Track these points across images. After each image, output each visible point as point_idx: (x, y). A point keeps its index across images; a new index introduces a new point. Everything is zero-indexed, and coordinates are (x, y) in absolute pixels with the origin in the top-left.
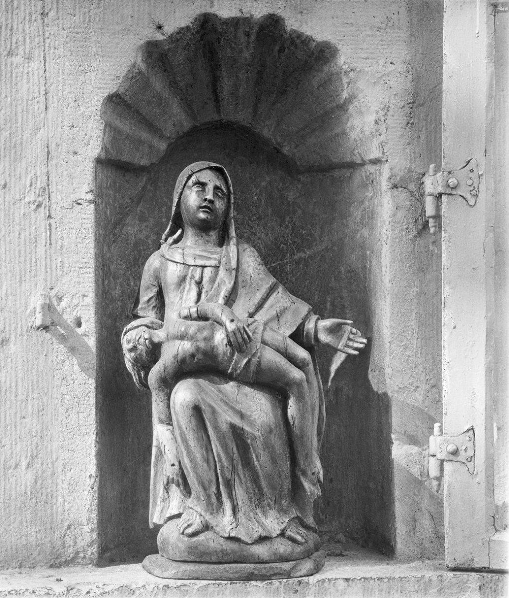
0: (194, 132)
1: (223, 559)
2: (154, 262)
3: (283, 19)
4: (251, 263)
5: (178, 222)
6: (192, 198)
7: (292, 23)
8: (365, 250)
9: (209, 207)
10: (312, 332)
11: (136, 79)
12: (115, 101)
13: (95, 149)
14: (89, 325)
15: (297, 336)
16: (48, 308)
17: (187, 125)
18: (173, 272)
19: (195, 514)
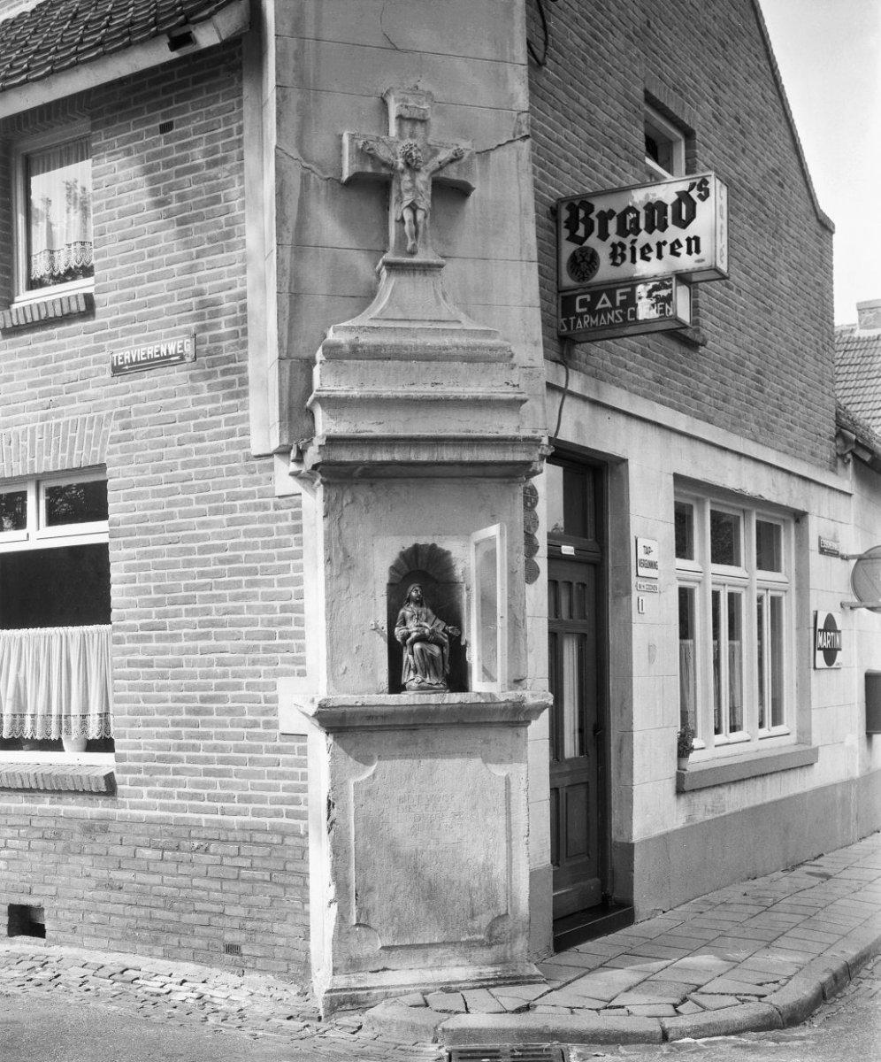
0: (410, 573)
1: (428, 689)
2: (401, 612)
3: (447, 553)
4: (429, 611)
5: (409, 600)
6: (414, 594)
7: (439, 546)
8: (478, 631)
9: (419, 597)
10: (503, 879)
11: (397, 562)
12: (392, 568)
13: (387, 581)
14: (386, 629)
15: (444, 630)
16: (376, 624)
17: (408, 570)
18: (408, 613)
19: (419, 678)
